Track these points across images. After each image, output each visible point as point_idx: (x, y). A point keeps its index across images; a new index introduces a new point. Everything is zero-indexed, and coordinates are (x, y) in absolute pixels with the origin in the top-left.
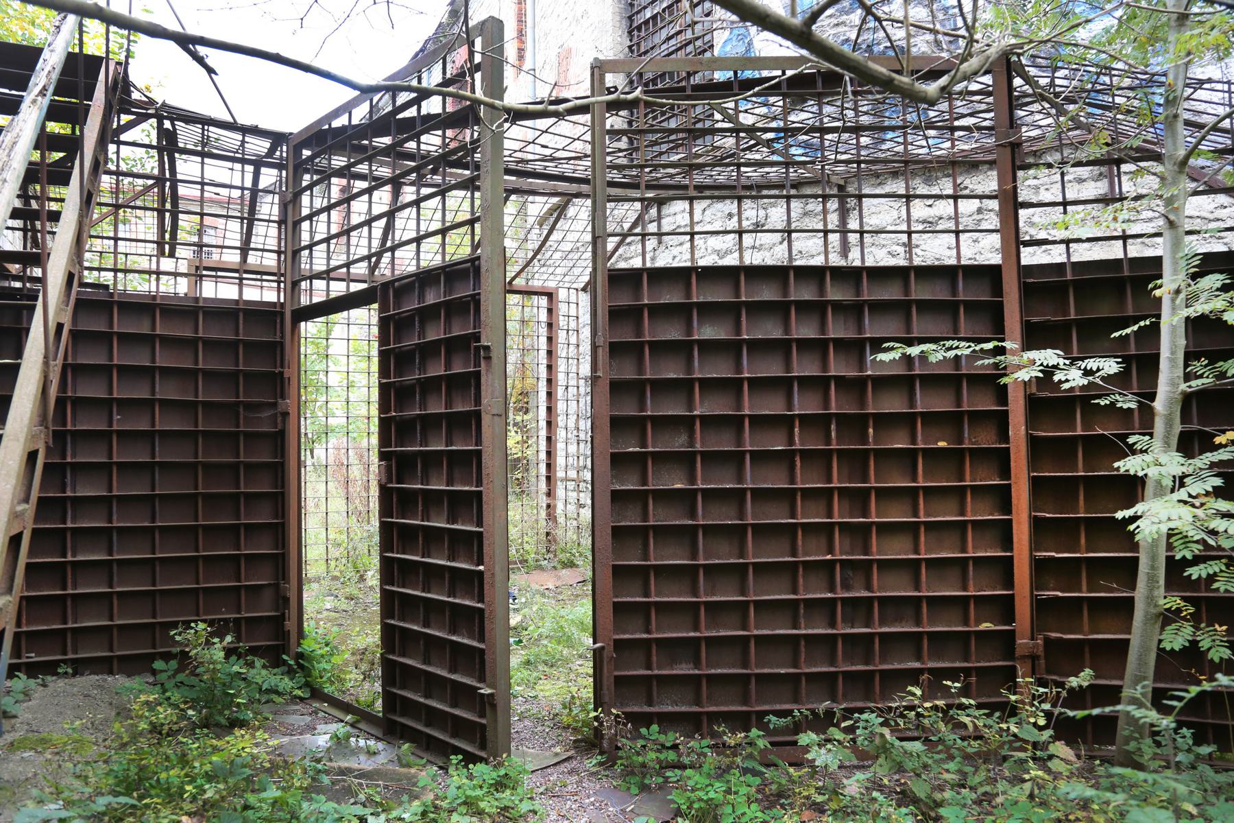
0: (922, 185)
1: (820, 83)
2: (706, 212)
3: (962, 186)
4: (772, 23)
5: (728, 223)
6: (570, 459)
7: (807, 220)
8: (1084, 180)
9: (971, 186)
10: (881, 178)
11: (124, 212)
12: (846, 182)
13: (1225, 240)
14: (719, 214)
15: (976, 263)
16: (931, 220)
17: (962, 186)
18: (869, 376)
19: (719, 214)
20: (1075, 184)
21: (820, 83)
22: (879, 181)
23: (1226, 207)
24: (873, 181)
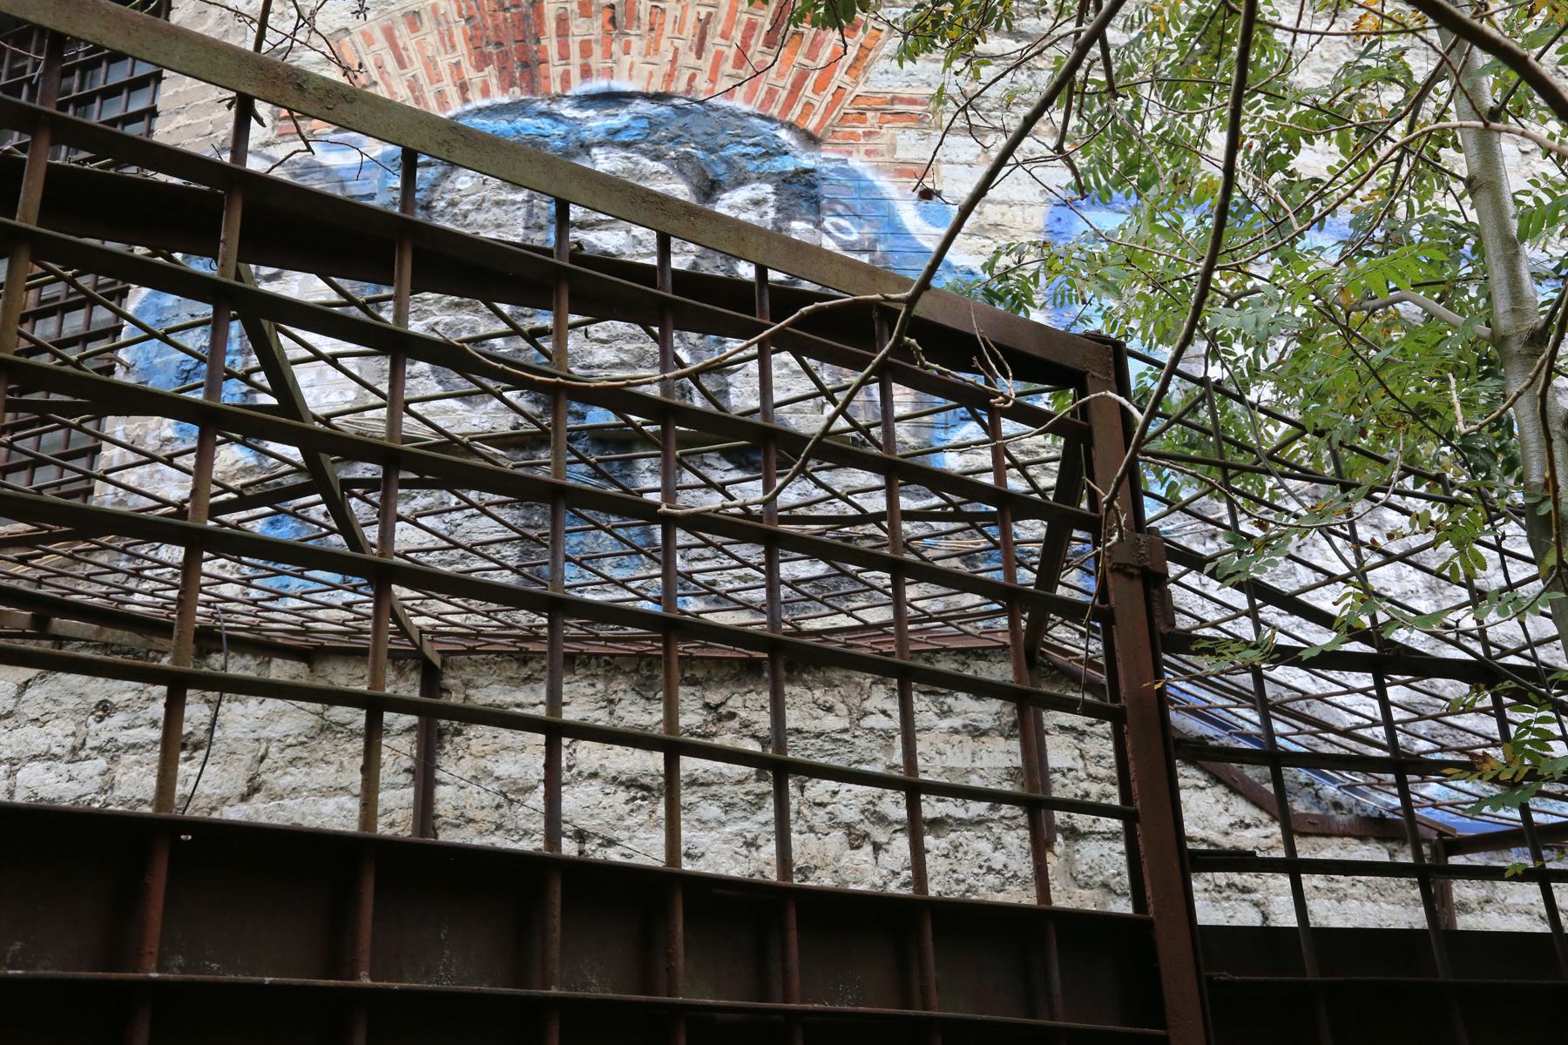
0: (631, 696)
1: (230, 234)
2: (29, 693)
3: (723, 710)
4: (426, 759)
5: (94, 727)
6: (863, 196)
7: (327, 745)
8: (985, 733)
9: (743, 714)
10: (534, 665)
11: (1113, 836)
12: (444, 663)
13: (1256, 896)
14: (70, 702)
15: (300, 704)
16: (647, 781)
17: (723, 710)
18: (555, 1000)
19: (70, 702)
20: (966, 738)
21: (230, 234)
22: (525, 672)
23: (1248, 826)
24: (511, 669)
